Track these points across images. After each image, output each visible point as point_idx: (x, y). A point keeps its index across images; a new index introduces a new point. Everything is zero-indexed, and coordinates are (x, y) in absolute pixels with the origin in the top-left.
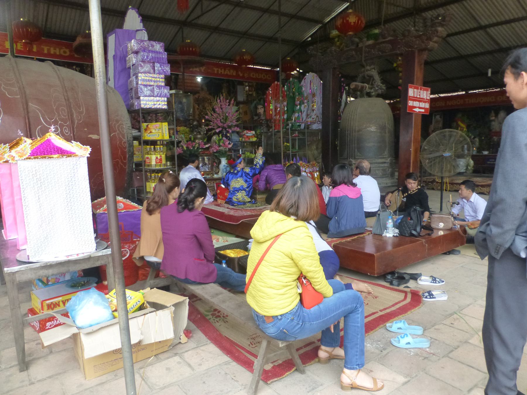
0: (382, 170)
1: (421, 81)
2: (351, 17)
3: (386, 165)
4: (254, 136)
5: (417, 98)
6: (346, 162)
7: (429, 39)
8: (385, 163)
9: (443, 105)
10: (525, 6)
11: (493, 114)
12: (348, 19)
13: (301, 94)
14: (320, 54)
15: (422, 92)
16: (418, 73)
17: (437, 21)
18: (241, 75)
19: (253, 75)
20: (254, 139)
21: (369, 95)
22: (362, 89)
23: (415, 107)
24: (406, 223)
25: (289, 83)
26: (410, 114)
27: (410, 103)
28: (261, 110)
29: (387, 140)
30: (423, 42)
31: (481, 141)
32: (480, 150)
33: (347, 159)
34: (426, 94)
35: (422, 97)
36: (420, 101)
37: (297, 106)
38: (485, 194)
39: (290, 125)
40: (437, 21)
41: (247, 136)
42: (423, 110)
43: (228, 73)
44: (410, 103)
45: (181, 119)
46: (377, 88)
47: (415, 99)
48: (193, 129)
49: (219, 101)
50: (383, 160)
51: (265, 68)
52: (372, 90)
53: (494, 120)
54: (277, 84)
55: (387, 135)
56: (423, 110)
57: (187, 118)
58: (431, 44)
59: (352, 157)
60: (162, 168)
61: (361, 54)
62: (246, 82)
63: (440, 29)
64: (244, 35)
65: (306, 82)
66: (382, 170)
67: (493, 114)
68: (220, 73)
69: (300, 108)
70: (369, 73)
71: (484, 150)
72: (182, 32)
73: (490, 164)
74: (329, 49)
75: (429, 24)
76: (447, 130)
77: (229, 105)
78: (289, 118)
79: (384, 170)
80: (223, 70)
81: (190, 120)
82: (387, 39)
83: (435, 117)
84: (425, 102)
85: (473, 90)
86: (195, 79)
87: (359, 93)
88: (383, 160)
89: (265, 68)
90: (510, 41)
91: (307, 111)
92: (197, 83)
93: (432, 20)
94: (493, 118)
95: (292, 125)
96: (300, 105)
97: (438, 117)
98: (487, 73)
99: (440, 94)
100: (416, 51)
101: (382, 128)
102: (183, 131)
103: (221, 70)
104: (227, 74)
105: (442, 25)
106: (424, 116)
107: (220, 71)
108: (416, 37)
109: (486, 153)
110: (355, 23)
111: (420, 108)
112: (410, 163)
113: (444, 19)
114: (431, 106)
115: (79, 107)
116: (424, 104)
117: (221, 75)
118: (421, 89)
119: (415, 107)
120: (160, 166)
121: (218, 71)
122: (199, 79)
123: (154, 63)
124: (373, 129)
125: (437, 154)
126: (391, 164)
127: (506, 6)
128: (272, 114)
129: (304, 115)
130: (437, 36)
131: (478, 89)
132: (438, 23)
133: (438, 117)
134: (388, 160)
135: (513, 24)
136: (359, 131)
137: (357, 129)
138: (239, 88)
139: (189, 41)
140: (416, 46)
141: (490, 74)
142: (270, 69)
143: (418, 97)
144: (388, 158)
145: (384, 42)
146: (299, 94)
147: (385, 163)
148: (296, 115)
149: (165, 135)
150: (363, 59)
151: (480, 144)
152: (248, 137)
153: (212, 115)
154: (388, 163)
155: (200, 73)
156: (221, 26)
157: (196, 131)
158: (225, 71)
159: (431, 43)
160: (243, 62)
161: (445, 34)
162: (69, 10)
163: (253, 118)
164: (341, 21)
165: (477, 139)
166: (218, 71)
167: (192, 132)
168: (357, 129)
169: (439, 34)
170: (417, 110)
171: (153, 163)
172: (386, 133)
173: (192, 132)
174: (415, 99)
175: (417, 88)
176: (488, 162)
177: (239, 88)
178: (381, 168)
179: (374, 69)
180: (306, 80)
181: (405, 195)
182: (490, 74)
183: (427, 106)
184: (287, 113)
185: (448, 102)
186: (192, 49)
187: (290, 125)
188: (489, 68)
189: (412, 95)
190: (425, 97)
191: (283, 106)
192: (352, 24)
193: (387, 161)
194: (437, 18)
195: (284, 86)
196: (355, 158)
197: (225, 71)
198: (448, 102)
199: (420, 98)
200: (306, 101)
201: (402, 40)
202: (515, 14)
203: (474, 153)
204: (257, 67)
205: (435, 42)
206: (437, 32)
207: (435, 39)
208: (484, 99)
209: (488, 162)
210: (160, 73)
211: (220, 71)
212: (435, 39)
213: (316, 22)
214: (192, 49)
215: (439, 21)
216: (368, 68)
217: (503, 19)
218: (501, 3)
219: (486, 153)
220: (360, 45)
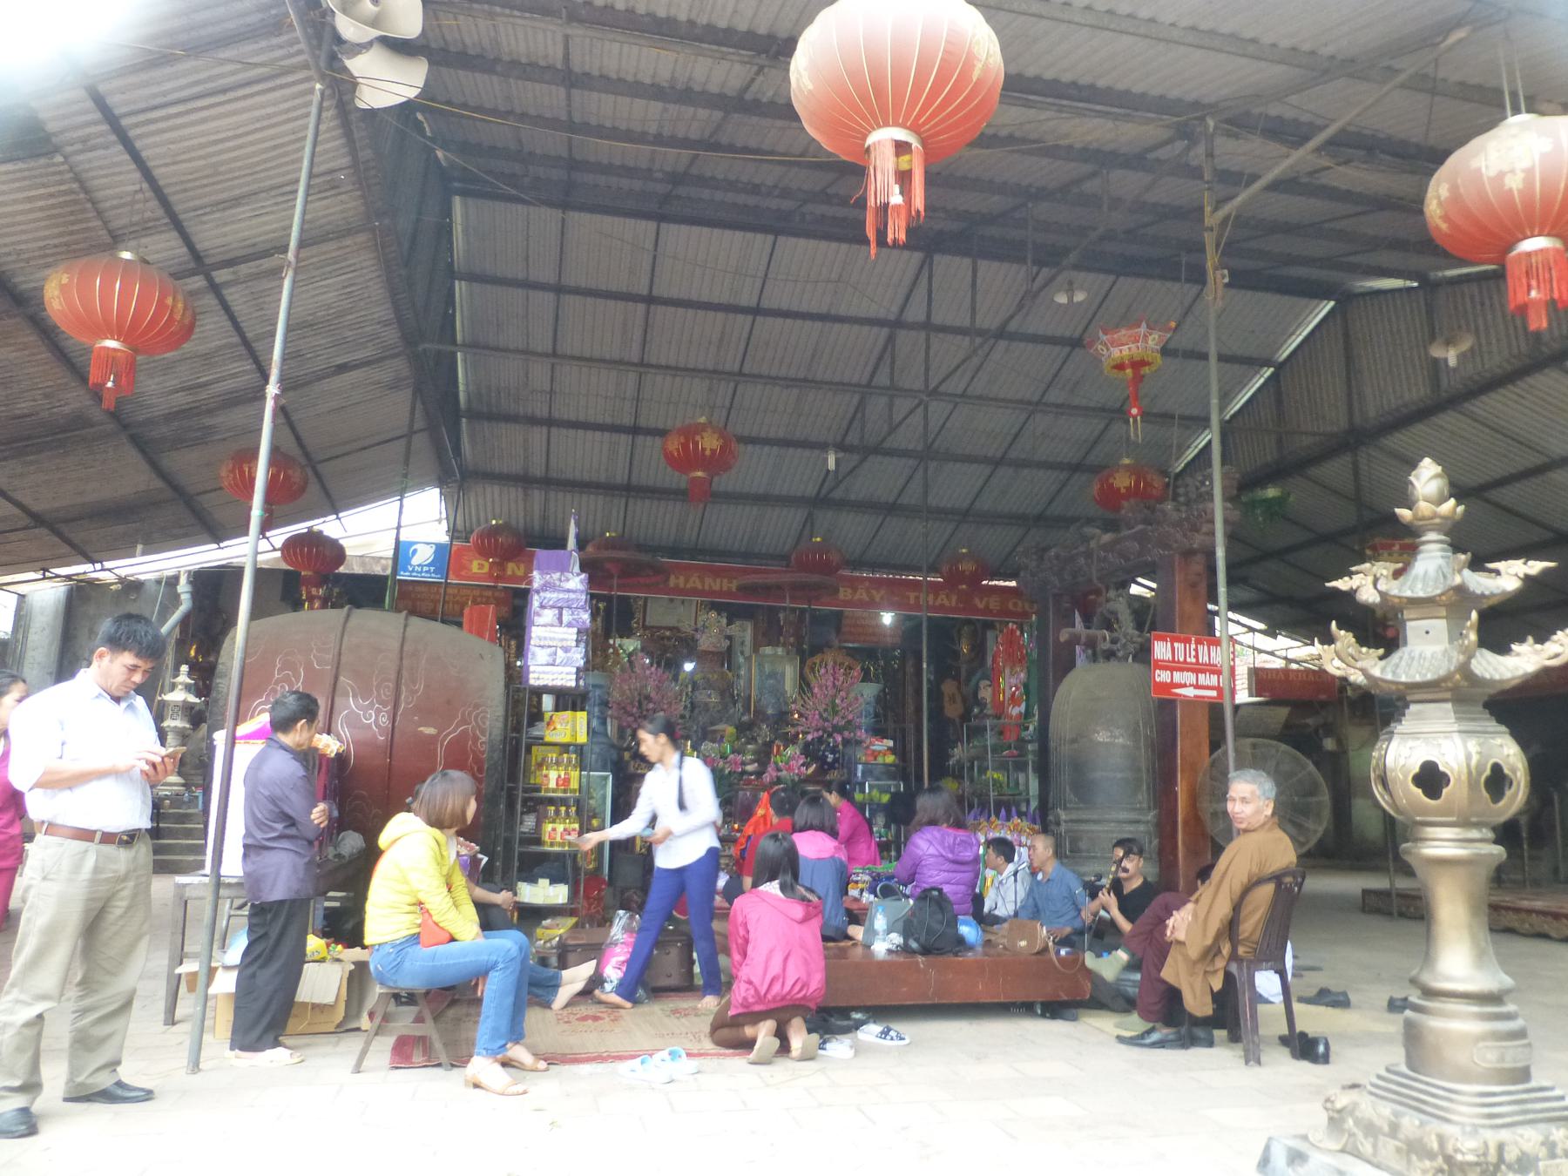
3: (1142, 828)
4: (892, 750)
8: (1138, 822)
18: (981, 606)
19: (1015, 604)
20: (890, 759)
21: (1110, 655)
22: (1091, 644)
27: (1163, 676)
35: (1204, 659)
36: (1172, 670)
42: (1214, 693)
43: (946, 602)
45: (770, 711)
47: (1173, 666)
50: (1133, 816)
56: (1214, 693)
64: (964, 515)
70: (1111, 605)
86: (878, 616)
92: (882, 626)
100: (1177, 557)
104: (942, 606)
108: (1178, 524)
111: (1197, 687)
112: (1175, 822)
115: (414, 683)
118: (1198, 642)
119: (1185, 686)
120: (565, 791)
122: (887, 618)
123: (561, 609)
136: (1074, 741)
147: (1138, 822)
152: (875, 754)
158: (687, 581)
160: (974, 580)
162: (584, 497)
170: (1190, 692)
171: (552, 785)
174: (1173, 666)
175: (1187, 641)
189: (1169, 656)
196: (1065, 809)
204: (1002, 583)
210: (570, 625)
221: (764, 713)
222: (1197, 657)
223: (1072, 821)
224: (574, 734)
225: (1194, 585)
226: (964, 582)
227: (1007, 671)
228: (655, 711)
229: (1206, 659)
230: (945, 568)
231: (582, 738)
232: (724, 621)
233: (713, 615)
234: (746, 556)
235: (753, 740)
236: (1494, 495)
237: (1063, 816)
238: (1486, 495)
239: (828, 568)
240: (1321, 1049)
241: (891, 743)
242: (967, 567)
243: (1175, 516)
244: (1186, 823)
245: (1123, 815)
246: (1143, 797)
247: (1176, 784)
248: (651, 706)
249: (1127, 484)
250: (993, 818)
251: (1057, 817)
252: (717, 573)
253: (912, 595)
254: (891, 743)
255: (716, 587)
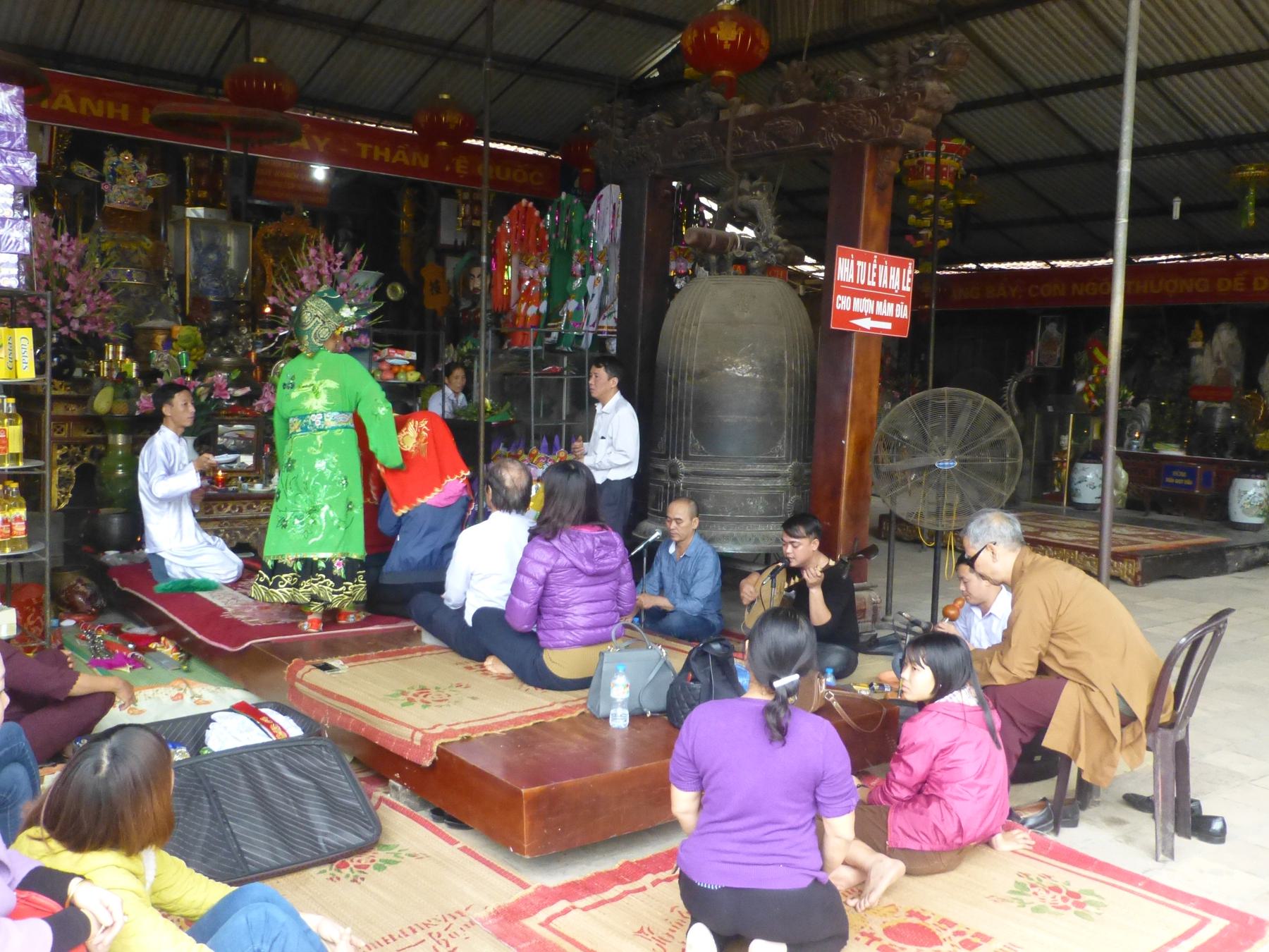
0: (768, 497)
1: (880, 237)
2: (721, 24)
3: (779, 482)
5: (865, 286)
6: (663, 467)
7: (903, 114)
8: (776, 476)
9: (1062, 293)
10: (1261, 20)
11: (1198, 331)
12: (713, 30)
13: (585, 242)
14: (619, 131)
15: (883, 269)
16: (874, 214)
17: (922, 61)
20: (413, 376)
23: (861, 315)
24: (683, 688)
25: (558, 208)
26: (844, 337)
28: (479, 282)
29: (785, 406)
30: (886, 121)
31: (1157, 410)
32: (1152, 436)
33: (666, 456)
34: (898, 277)
35: (883, 283)
36: (876, 298)
37: (575, 277)
38: (1124, 582)
39: (555, 335)
40: (922, 61)
41: (392, 365)
42: (888, 326)
43: (405, 160)
44: (842, 303)
46: (764, 249)
47: (856, 291)
48: (211, 334)
49: (312, 252)
50: (771, 469)
51: (530, 151)
52: (753, 253)
53: (1201, 352)
54: (526, 208)
55: (786, 392)
56: (888, 326)
57: (232, 295)
58: (906, 129)
59: (679, 452)
60: (21, 465)
61: (724, 142)
62: (464, 190)
63: (931, 85)
65: (602, 207)
66: (768, 497)
67: (1198, 331)
68: (376, 157)
69: (584, 286)
71: (1165, 439)
72: (247, 35)
73: (1174, 485)
74: (643, 120)
75: (903, 68)
76: (946, 389)
77: (344, 267)
78: (552, 315)
79: (773, 499)
80: (387, 150)
81: (238, 303)
82: (792, 105)
83: (1043, 329)
84: (895, 301)
85: (1152, 254)
86: (306, 171)
87: (713, 258)
88: (771, 469)
89: (530, 151)
90: (1235, 120)
91: (602, 299)
92: (314, 184)
93: (912, 59)
94: (1197, 345)
95: (560, 335)
96: (584, 275)
97: (1052, 328)
98: (1169, 211)
99: (1057, 259)
101: (774, 369)
102: (188, 339)
103: (382, 149)
105: (941, 77)
106: (888, 344)
107: (377, 154)
108: (875, 104)
109: (1173, 451)
110: (733, 43)
113: (941, 59)
114: (914, 315)
116: (891, 306)
117: (381, 164)
118: (880, 262)
119: (861, 315)
121: (371, 152)
122: (319, 173)
124: (741, 370)
125: (921, 461)
126: (795, 479)
127: (1206, 16)
128: (509, 296)
129: (593, 306)
130: (925, 106)
131: (1167, 253)
132: (928, 67)
133: (1052, 328)
134: (788, 469)
135: (1234, 70)
136: (702, 374)
137: (695, 368)
138: (446, 205)
139: (262, 60)
140: (866, 133)
141: (1176, 214)
142: (541, 154)
143: (872, 283)
144: (788, 460)
145: (783, 113)
146: (583, 242)
147: (776, 476)
148: (572, 305)
149: (20, 366)
150: (729, 156)
151: (1153, 421)
153: (288, 294)
154: (785, 476)
155: (325, 158)
156: (373, 20)
157: (218, 344)
158: (392, 154)
159: (907, 125)
161: (950, 102)
163: (458, 304)
164: (695, 34)
165: (1146, 407)
166: (371, 152)
167: (208, 344)
168: (695, 368)
169: (927, 100)
170: (866, 323)
172: (782, 386)
173: (208, 344)
174: (856, 291)
175: (869, 260)
176: (1170, 480)
177: (446, 205)
178: (764, 492)
179: (760, 188)
180: (602, 202)
181: (792, 582)
182: (1176, 214)
183: (903, 312)
184: (549, 298)
185: (1075, 286)
186: (269, 86)
187: (555, 335)
188: (1176, 194)
189: (850, 278)
190: (895, 285)
191: (537, 272)
192: (727, 46)
193: (781, 471)
194: (924, 53)
195: (543, 217)
196: (686, 458)
197: (392, 154)
198: (1075, 286)
199: (877, 288)
200: (599, 265)
201: (830, 109)
202: (1236, 41)
203: (1135, 449)
205: (923, 123)
206: (923, 94)
207: (919, 114)
208: (1187, 285)
209: (1170, 480)
211: (377, 154)
212: (919, 114)
213: (676, 26)
214: (269, 86)
215: (930, 62)
216: (745, 185)
217: (1204, 54)
218: (1192, 8)
219: (1173, 451)
220: (724, 116)
221: (206, 302)
222: (877, 279)
223: (695, 473)
224: (12, 367)
225: (882, 188)
226: (438, 136)
227: (515, 259)
228: (75, 304)
229: (885, 282)
230: (423, 119)
231: (27, 372)
232: (144, 168)
233: (127, 157)
234: (136, 70)
235: (229, 350)
236: (1055, 102)
237: (683, 466)
238: (1046, 101)
239: (277, 102)
240: (1217, 826)
241: (413, 356)
242: (451, 119)
243: (868, 92)
244: (851, 483)
245: (760, 468)
246: (782, 446)
247: (843, 436)
248: (67, 295)
249: (733, 38)
250: (534, 450)
251: (674, 466)
252: (99, 92)
253: (364, 148)
254: (413, 356)
255: (98, 112)
